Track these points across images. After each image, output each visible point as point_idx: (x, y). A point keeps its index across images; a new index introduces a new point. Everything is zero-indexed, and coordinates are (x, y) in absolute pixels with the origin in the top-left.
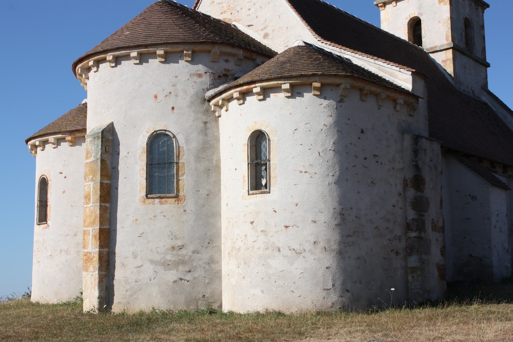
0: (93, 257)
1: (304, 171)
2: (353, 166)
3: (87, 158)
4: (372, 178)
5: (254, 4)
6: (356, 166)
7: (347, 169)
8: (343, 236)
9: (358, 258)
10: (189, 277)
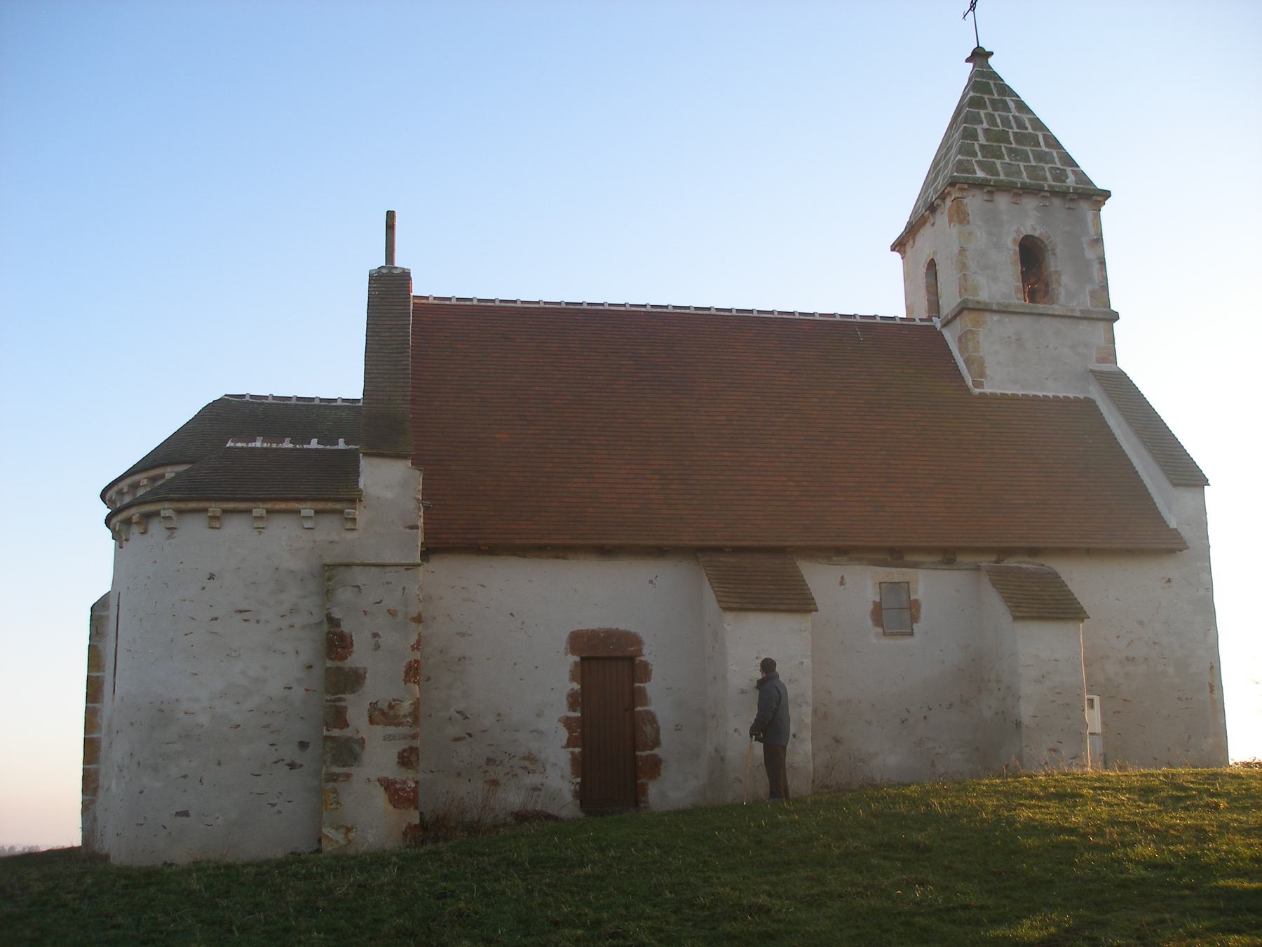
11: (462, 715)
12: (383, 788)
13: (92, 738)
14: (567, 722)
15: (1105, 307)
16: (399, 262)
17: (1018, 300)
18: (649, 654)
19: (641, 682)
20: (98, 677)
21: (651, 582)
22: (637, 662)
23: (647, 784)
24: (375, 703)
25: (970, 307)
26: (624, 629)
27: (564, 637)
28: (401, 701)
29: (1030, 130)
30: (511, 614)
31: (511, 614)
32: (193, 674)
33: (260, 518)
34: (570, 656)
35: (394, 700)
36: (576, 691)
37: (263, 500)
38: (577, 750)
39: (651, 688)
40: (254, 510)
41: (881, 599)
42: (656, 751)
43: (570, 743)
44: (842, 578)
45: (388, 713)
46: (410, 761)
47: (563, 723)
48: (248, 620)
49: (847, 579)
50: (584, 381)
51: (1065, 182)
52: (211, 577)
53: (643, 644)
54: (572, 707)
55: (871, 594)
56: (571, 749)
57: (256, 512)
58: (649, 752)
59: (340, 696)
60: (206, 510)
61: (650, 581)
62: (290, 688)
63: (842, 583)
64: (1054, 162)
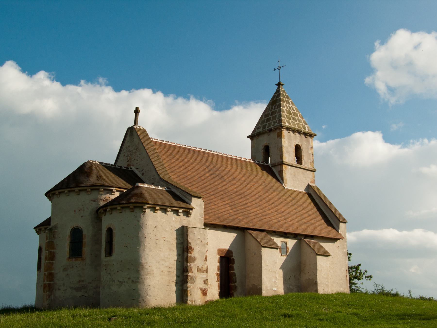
0: (47, 286)
1: (125, 246)
3: (46, 240)
5: (139, 158)
10: (86, 295)
13: (51, 273)
15: (313, 167)
17: (295, 163)
19: (233, 264)
20: (54, 252)
22: (231, 259)
25: (285, 163)
29: (296, 112)
33: (132, 209)
34: (218, 255)
37: (171, 207)
41: (281, 246)
42: (236, 284)
44: (349, 259)
51: (305, 130)
58: (234, 284)
64: (302, 123)
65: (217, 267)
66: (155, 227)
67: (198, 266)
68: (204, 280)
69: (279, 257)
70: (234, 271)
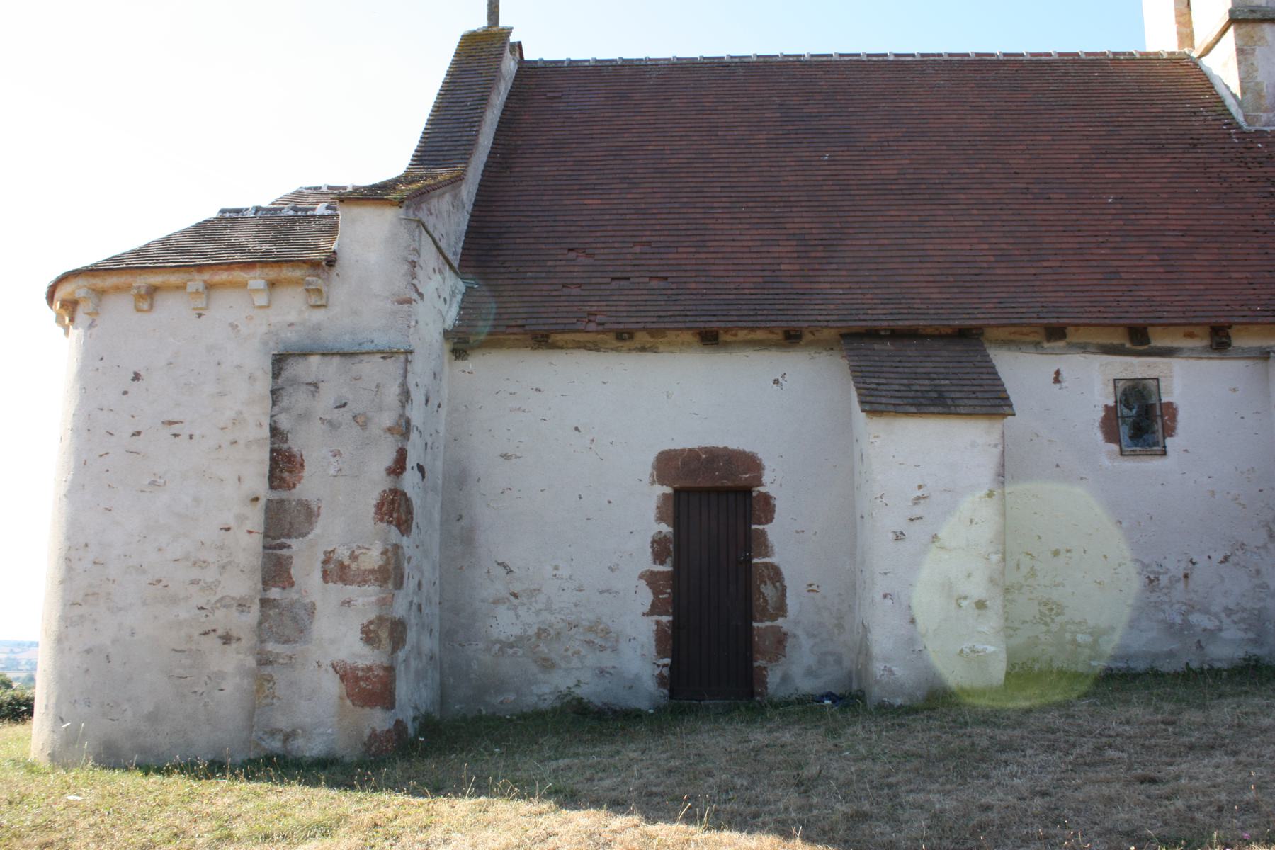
2: (101, 456)
4: (155, 474)
6: (107, 454)
7: (85, 464)
8: (65, 605)
9: (88, 651)
11: (505, 567)
12: (338, 676)
14: (651, 579)
16: (503, 22)
18: (770, 484)
21: (776, 382)
22: (754, 494)
23: (765, 668)
24: (330, 552)
26: (735, 448)
27: (651, 458)
28: (367, 549)
30: (577, 429)
31: (577, 429)
32: (106, 509)
35: (359, 547)
36: (665, 536)
38: (665, 619)
39: (774, 531)
40: (189, 283)
42: (780, 622)
43: (655, 609)
44: (1058, 373)
45: (349, 567)
46: (378, 637)
47: (646, 581)
48: (133, 435)
49: (1064, 375)
50: (713, 138)
52: (137, 377)
53: (763, 469)
54: (659, 557)
55: (1103, 396)
56: (656, 617)
57: (192, 287)
58: (768, 624)
59: (283, 540)
60: (129, 287)
61: (775, 380)
62: (228, 529)
63: (1057, 380)
65: (648, 544)
66: (133, 380)
67: (326, 553)
68: (365, 622)
69: (1106, 462)
70: (766, 555)
